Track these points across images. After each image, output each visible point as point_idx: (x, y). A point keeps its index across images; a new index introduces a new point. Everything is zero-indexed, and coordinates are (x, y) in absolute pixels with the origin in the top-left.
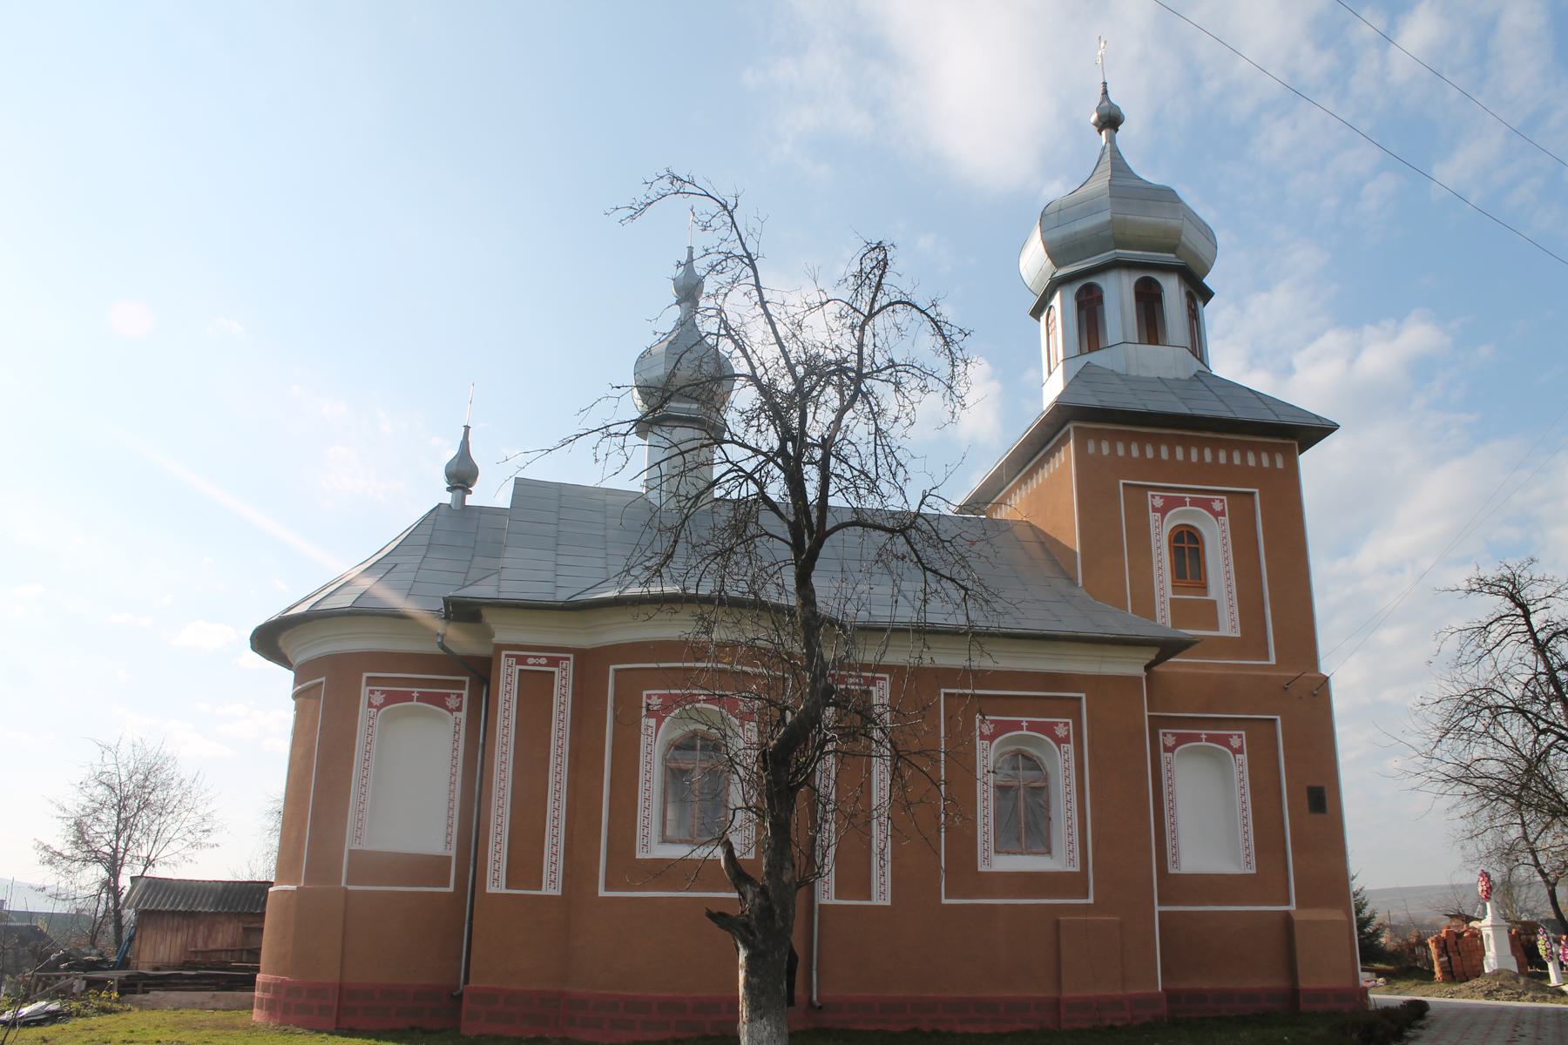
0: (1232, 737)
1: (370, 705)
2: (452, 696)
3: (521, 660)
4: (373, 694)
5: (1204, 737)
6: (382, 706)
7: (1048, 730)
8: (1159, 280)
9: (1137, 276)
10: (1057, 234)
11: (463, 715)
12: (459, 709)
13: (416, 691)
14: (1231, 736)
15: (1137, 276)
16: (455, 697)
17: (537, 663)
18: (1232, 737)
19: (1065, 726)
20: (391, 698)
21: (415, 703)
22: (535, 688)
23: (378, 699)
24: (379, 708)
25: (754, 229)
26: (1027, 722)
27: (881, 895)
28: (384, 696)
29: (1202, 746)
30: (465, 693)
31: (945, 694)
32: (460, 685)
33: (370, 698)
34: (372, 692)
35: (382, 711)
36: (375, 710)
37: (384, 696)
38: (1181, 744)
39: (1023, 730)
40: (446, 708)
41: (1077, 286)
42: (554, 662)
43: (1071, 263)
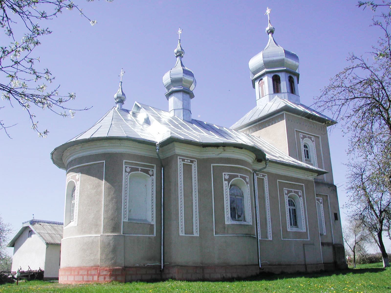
0: (150, 171)
1: (126, 171)
2: (128, 167)
3: (183, 160)
4: (127, 168)
5: (140, 169)
6: (130, 172)
7: (244, 178)
8: (293, 77)
9: (289, 75)
10: (266, 59)
11: (154, 177)
12: (153, 175)
13: (140, 168)
14: (149, 170)
15: (289, 75)
16: (129, 168)
17: (187, 162)
18: (150, 171)
19: (152, 171)
20: (132, 170)
21: (239, 178)
22: (187, 169)
23: (128, 170)
24: (129, 173)
25: (389, 24)
26: (140, 168)
27: (303, 227)
28: (229, 176)
29: (139, 173)
30: (155, 170)
31: (125, 162)
32: (153, 167)
33: (125, 169)
34: (126, 167)
35: (130, 174)
36: (128, 173)
37: (229, 176)
38: (132, 172)
39: (139, 171)
40: (149, 174)
41: (272, 75)
42: (192, 162)
43: (277, 67)
